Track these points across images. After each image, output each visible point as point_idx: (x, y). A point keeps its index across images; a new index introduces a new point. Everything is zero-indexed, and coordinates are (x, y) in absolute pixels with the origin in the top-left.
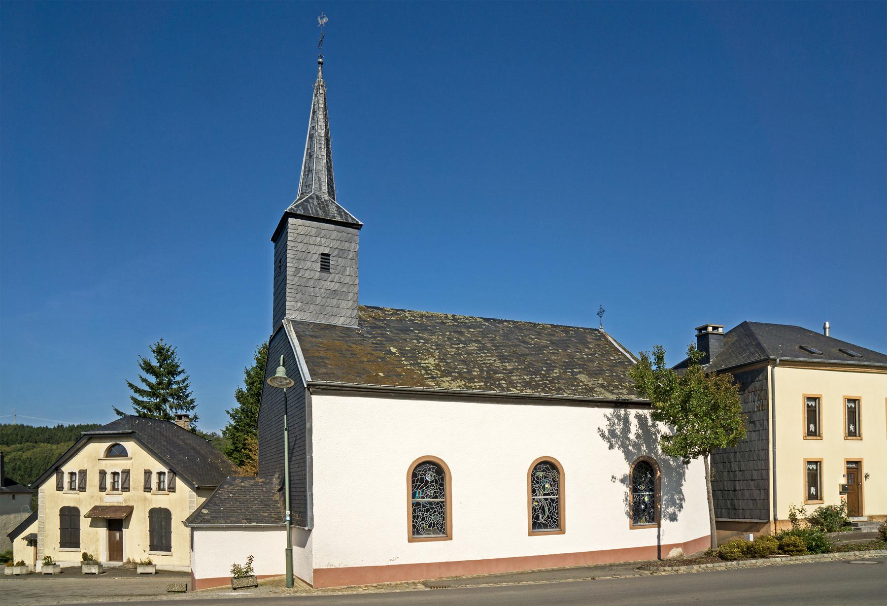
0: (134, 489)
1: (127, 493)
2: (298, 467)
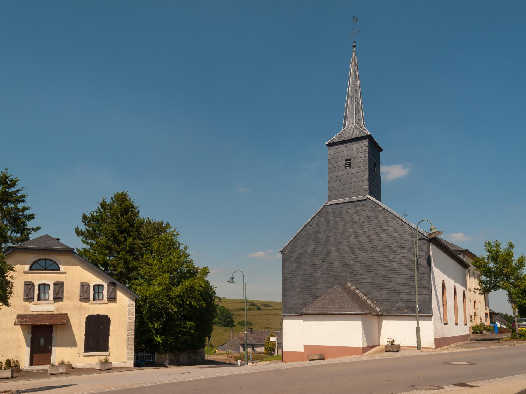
0: (68, 299)
1: (61, 303)
2: (355, 228)
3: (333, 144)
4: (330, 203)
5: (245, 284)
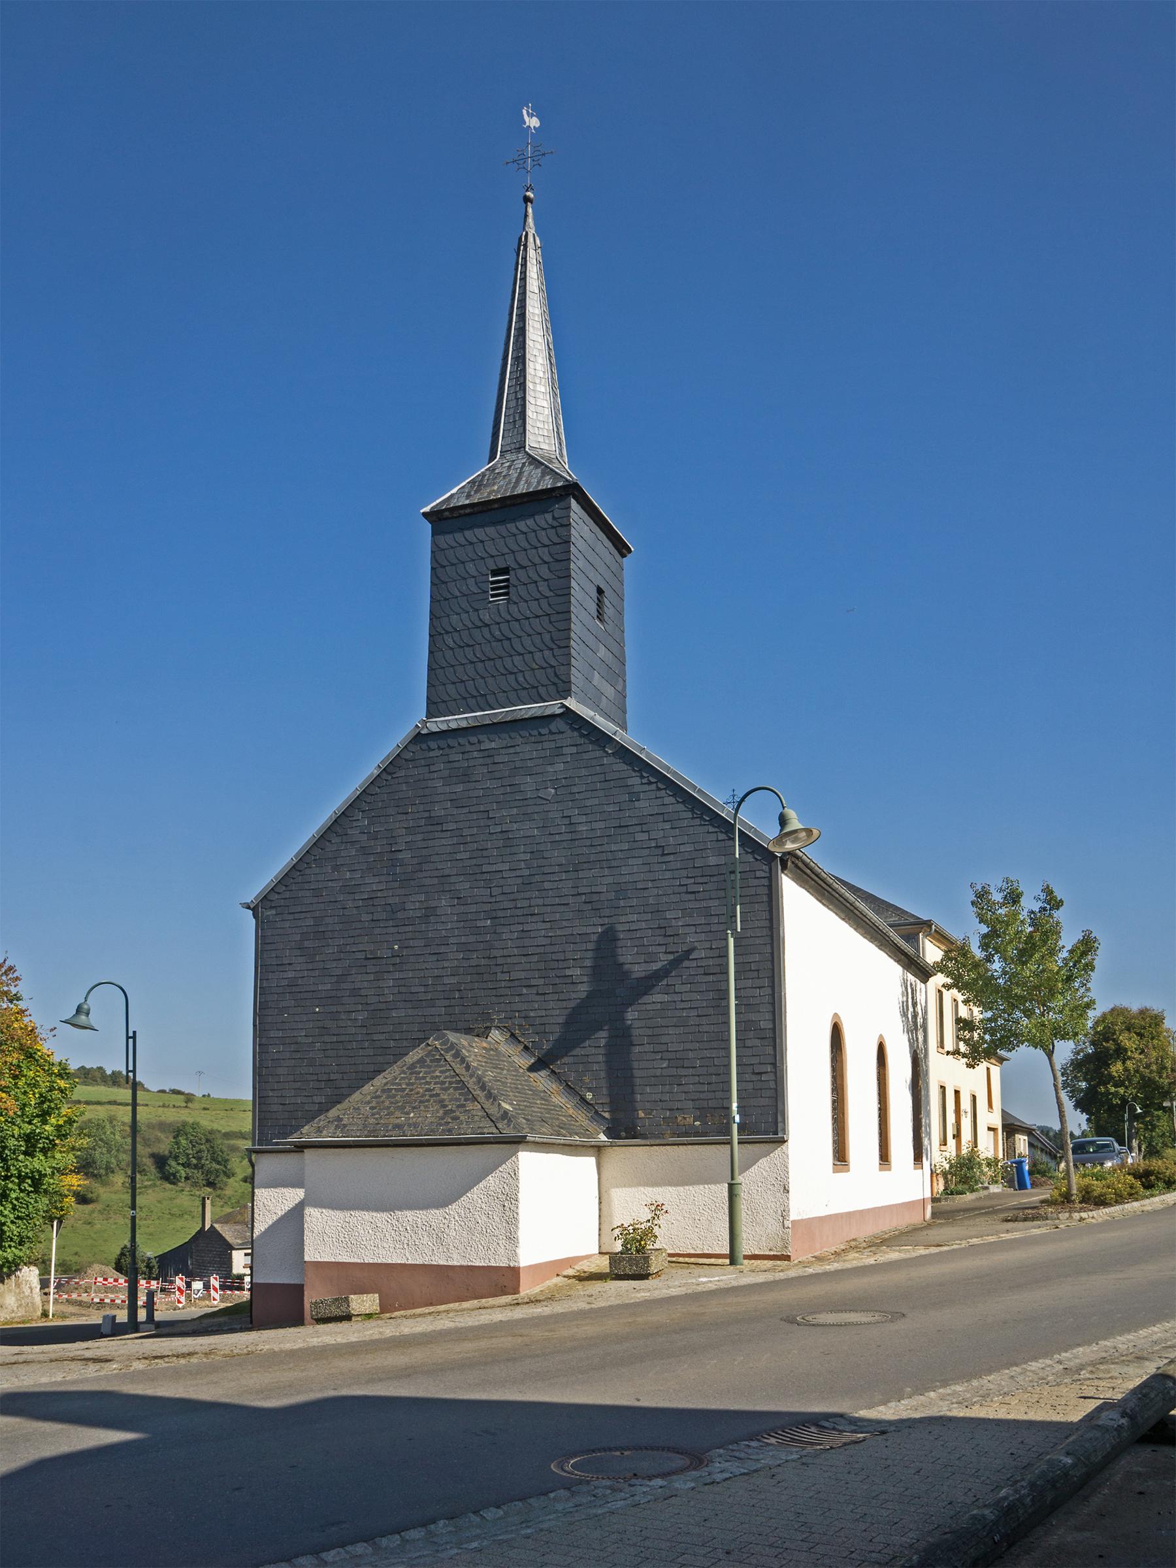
3: (447, 514)
4: (439, 724)
5: (131, 1034)
